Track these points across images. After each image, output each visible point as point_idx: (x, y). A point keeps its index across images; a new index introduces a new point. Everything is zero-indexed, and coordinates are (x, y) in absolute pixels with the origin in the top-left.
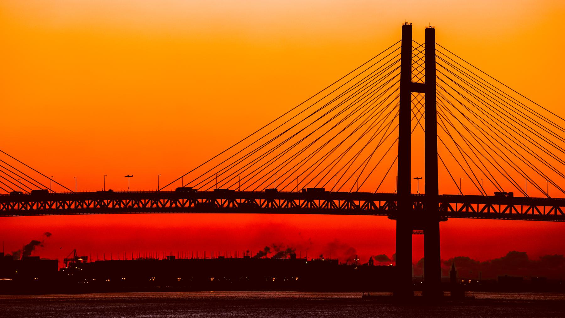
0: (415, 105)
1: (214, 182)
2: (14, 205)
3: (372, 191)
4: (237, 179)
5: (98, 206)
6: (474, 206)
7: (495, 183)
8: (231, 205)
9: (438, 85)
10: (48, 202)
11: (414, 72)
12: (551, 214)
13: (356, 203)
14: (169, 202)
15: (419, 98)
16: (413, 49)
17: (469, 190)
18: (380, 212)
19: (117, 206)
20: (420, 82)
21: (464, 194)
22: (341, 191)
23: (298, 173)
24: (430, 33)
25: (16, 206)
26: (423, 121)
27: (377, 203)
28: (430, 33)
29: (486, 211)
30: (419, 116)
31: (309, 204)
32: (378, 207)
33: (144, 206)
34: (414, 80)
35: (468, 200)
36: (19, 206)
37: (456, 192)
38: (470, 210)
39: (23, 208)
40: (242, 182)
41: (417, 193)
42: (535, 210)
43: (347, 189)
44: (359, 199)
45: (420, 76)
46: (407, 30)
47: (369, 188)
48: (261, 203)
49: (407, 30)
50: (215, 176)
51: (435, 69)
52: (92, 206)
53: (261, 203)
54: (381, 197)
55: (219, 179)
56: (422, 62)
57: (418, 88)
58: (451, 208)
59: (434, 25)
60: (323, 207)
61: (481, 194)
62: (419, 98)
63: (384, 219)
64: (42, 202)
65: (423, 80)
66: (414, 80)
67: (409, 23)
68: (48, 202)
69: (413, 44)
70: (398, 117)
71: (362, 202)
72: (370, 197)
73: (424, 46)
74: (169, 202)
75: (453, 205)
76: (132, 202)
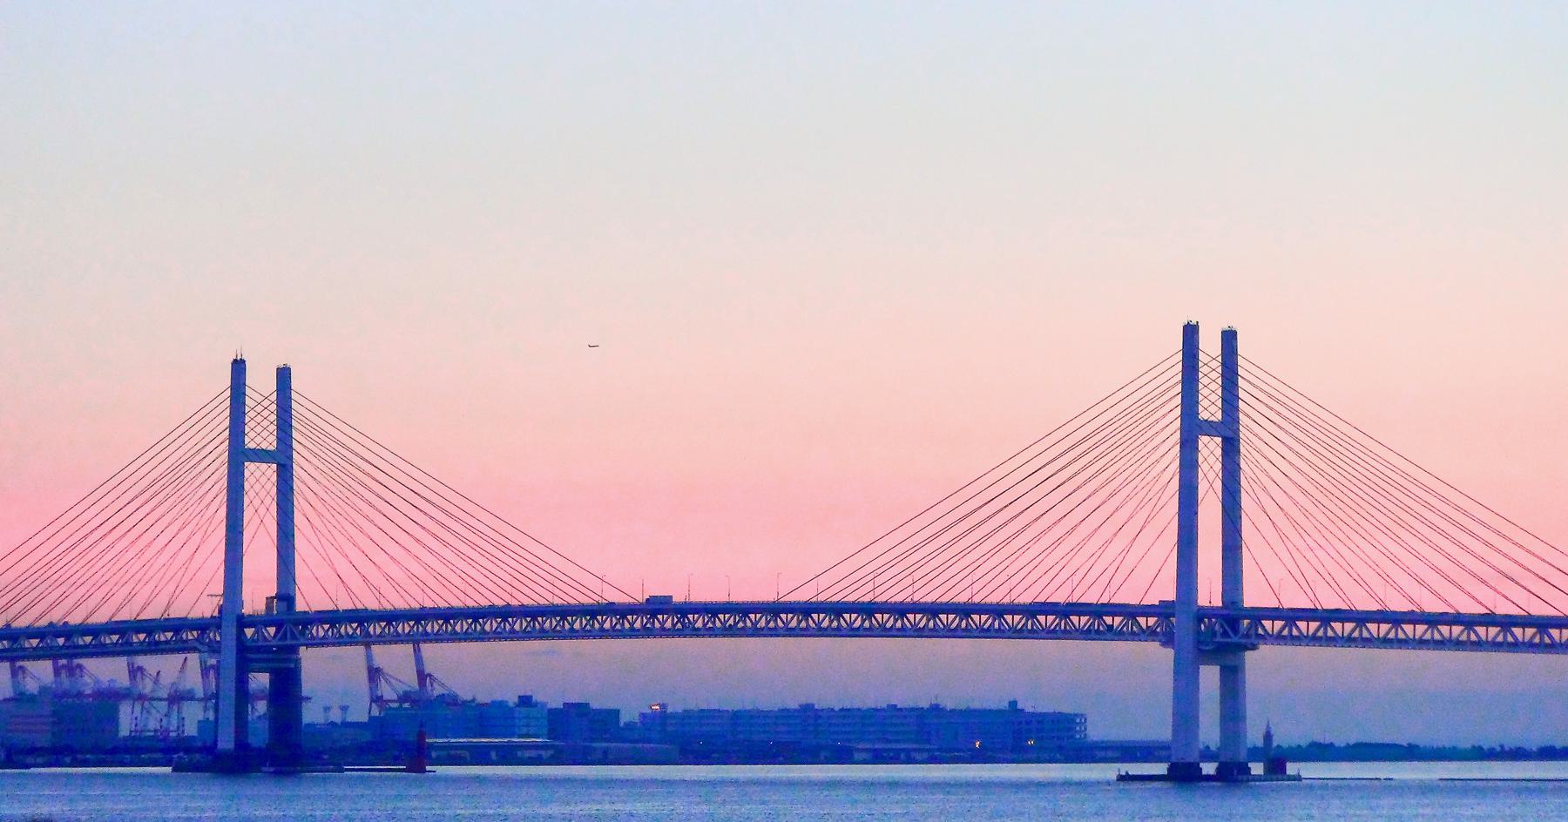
0: (1211, 470)
1: (870, 586)
2: (544, 622)
3: (1134, 601)
4: (909, 581)
5: (679, 625)
6: (1302, 625)
7: (1339, 591)
8: (931, 624)
9: (1247, 440)
10: (659, 616)
11: (1203, 403)
12: (792, 615)
13: (1108, 620)
14: (827, 618)
15: (1212, 445)
16: (1200, 364)
17: (1295, 599)
18: (1150, 634)
19: (618, 627)
20: (1212, 419)
21: (1286, 605)
22: (1082, 600)
23: (1010, 571)
24: (1229, 339)
25: (547, 625)
26: (1218, 485)
27: (1142, 620)
28: (1229, 339)
29: (1285, 632)
30: (1211, 476)
31: (1063, 622)
32: (1144, 627)
33: (754, 624)
34: (1204, 415)
35: (1292, 616)
36: (551, 622)
37: (1272, 603)
38: (1547, 640)
39: (588, 626)
40: (917, 585)
41: (1208, 605)
42: (1364, 630)
43: (1092, 598)
44: (1113, 615)
45: (1213, 409)
46: (1191, 332)
47: (1129, 596)
48: (982, 622)
49: (1191, 332)
50: (871, 576)
51: (1237, 408)
52: (668, 625)
53: (982, 622)
54: (1147, 611)
55: (878, 581)
56: (1216, 376)
57: (1210, 428)
58: (1263, 627)
59: (1236, 327)
60: (1053, 627)
61: (1313, 607)
62: (1212, 445)
63: (1153, 647)
64: (618, 617)
65: (1219, 416)
66: (1204, 415)
67: (1194, 322)
68: (659, 616)
69: (1201, 356)
70: (1177, 477)
71: (1118, 620)
72: (1130, 612)
73: (1220, 359)
74: (827, 618)
75: (1267, 624)
76: (735, 618)
